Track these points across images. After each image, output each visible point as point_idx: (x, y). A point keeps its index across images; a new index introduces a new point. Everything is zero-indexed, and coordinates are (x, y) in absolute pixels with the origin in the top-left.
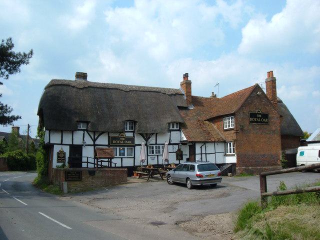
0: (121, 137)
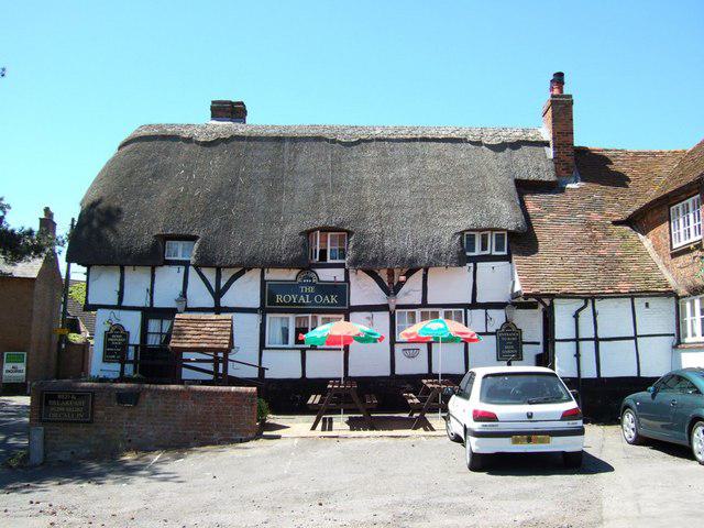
0: (304, 284)
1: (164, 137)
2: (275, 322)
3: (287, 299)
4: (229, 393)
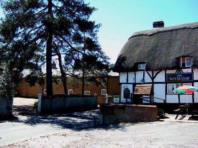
1: (139, 35)
2: (170, 86)
3: (173, 79)
4: (148, 107)
